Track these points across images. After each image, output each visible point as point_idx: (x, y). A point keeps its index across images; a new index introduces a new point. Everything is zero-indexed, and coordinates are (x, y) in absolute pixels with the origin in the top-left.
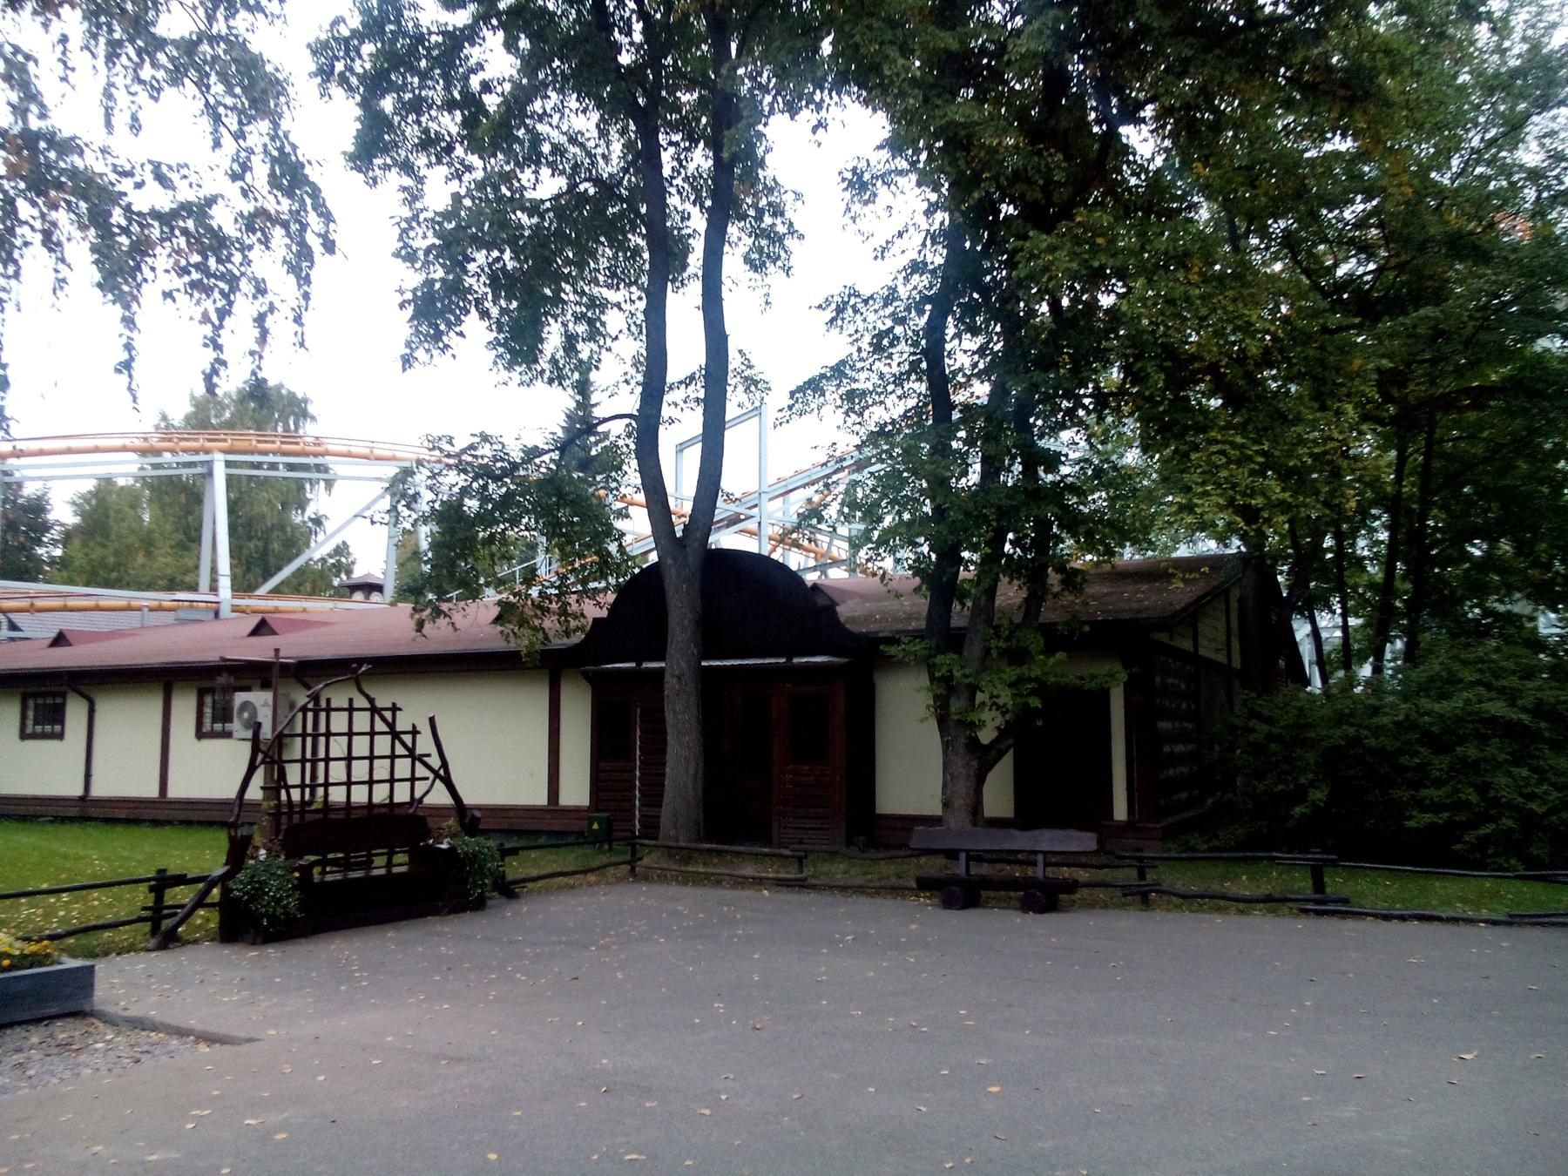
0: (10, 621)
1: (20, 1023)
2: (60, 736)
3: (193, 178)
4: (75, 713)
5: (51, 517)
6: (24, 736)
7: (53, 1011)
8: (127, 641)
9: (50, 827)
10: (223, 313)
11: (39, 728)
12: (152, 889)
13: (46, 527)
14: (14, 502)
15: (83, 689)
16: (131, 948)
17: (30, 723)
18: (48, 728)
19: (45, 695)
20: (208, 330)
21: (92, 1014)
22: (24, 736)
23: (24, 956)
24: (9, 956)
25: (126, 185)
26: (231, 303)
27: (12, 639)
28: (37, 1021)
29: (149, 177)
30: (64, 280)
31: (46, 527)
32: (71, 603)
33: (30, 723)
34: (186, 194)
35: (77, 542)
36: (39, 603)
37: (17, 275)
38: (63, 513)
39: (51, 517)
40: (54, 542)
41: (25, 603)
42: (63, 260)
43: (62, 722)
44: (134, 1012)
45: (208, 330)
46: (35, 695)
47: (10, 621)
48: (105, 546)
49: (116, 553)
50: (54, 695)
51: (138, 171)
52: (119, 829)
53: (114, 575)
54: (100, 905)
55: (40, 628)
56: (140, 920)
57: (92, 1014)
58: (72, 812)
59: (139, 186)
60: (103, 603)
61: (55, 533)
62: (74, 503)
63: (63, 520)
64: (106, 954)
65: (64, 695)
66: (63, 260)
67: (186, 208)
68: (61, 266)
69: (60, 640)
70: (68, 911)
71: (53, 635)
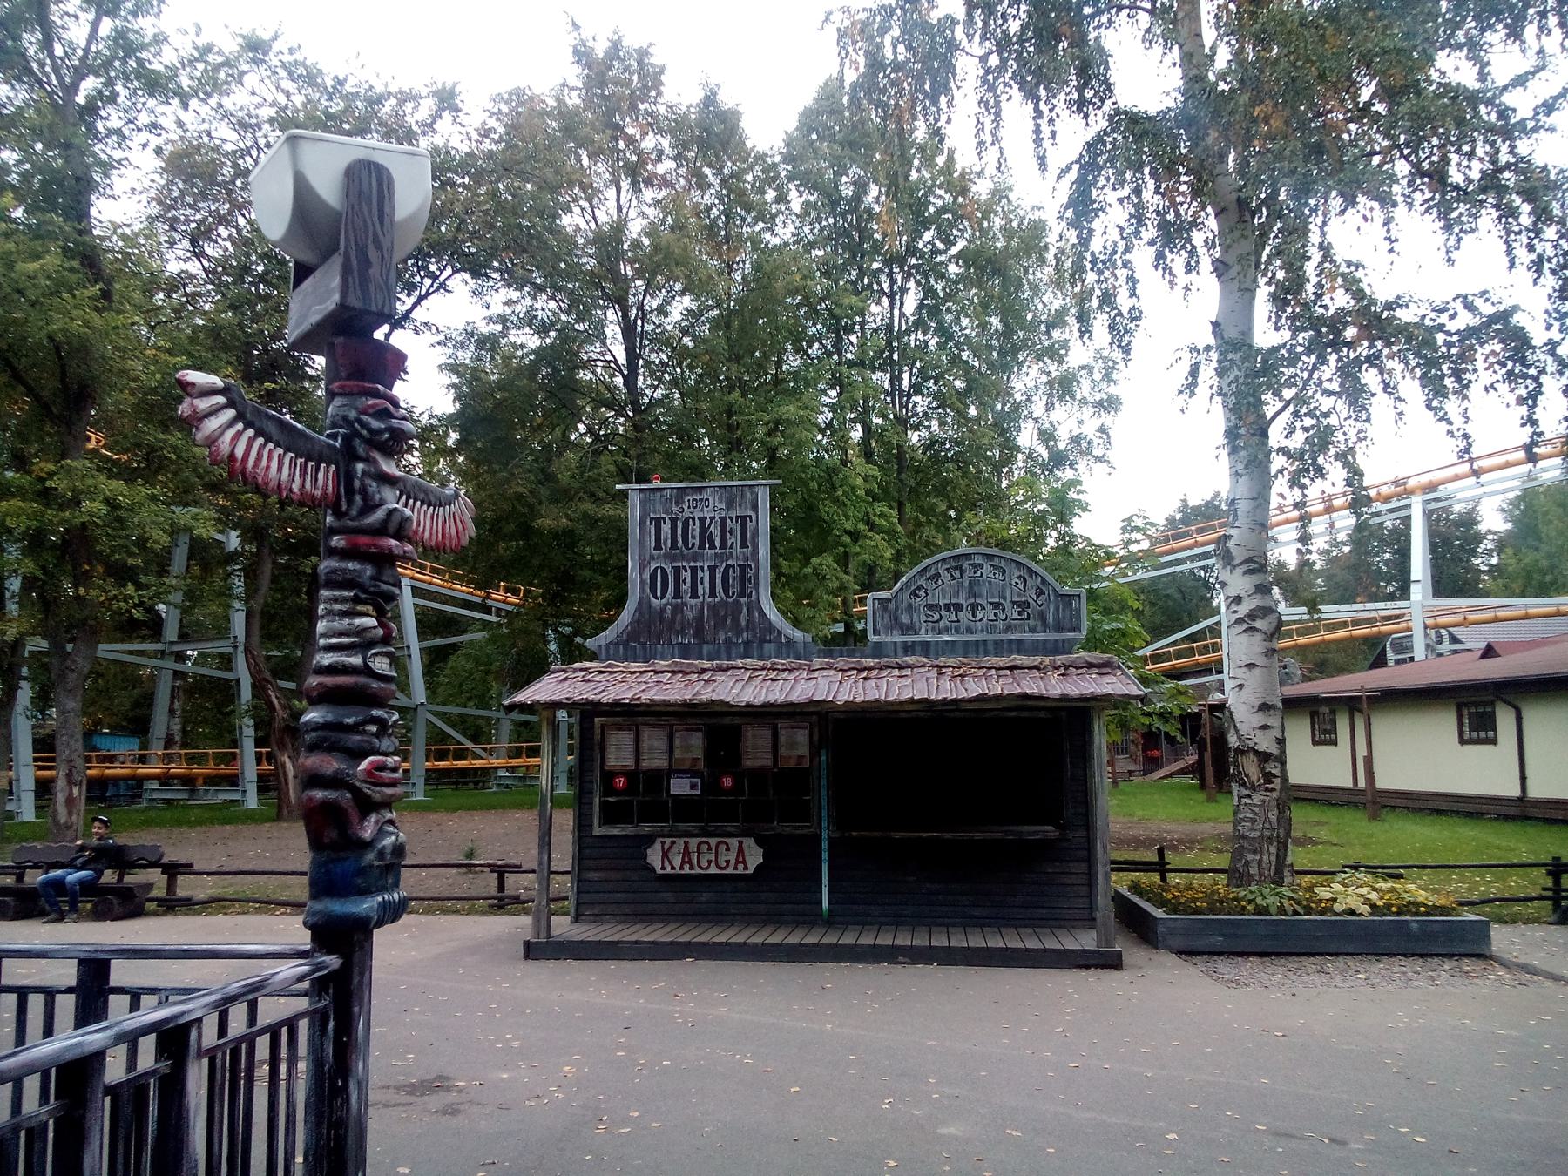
0: (1450, 634)
1: (1438, 955)
2: (1335, 743)
3: (1494, 299)
4: (1505, 721)
5: (1482, 528)
6: (1463, 741)
7: (1462, 950)
8: (1548, 651)
9: (1497, 825)
10: (1534, 396)
11: (1475, 734)
12: (1549, 873)
13: (1479, 538)
14: (1447, 519)
15: (1510, 698)
16: (1536, 920)
17: (1466, 729)
18: (1482, 734)
19: (1476, 704)
20: (1524, 410)
21: (1491, 958)
22: (1463, 741)
23: (1435, 907)
24: (1425, 905)
25: (1444, 318)
26: (1540, 385)
27: (1456, 652)
28: (1450, 956)
29: (1459, 305)
30: (1401, 413)
31: (1479, 538)
32: (1502, 614)
33: (1466, 729)
34: (1487, 310)
35: (1509, 551)
36: (1472, 617)
37: (1368, 420)
38: (1493, 521)
39: (1482, 528)
40: (1489, 553)
41: (1459, 618)
42: (1399, 399)
43: (1494, 730)
44: (1522, 960)
45: (1524, 410)
46: (1466, 705)
47: (1450, 634)
48: (1537, 550)
49: (1549, 556)
50: (1485, 704)
51: (1452, 305)
52: (1555, 828)
53: (1548, 578)
54: (1516, 884)
55: (1475, 639)
56: (1542, 898)
57: (1491, 958)
58: (1513, 811)
59: (1452, 317)
60: (1532, 611)
61: (1488, 544)
62: (1503, 510)
63: (1495, 528)
64: (1514, 922)
65: (1492, 704)
66: (1399, 399)
67: (1493, 319)
68: (1398, 404)
69: (1489, 652)
70: (1486, 885)
71: (1483, 645)
